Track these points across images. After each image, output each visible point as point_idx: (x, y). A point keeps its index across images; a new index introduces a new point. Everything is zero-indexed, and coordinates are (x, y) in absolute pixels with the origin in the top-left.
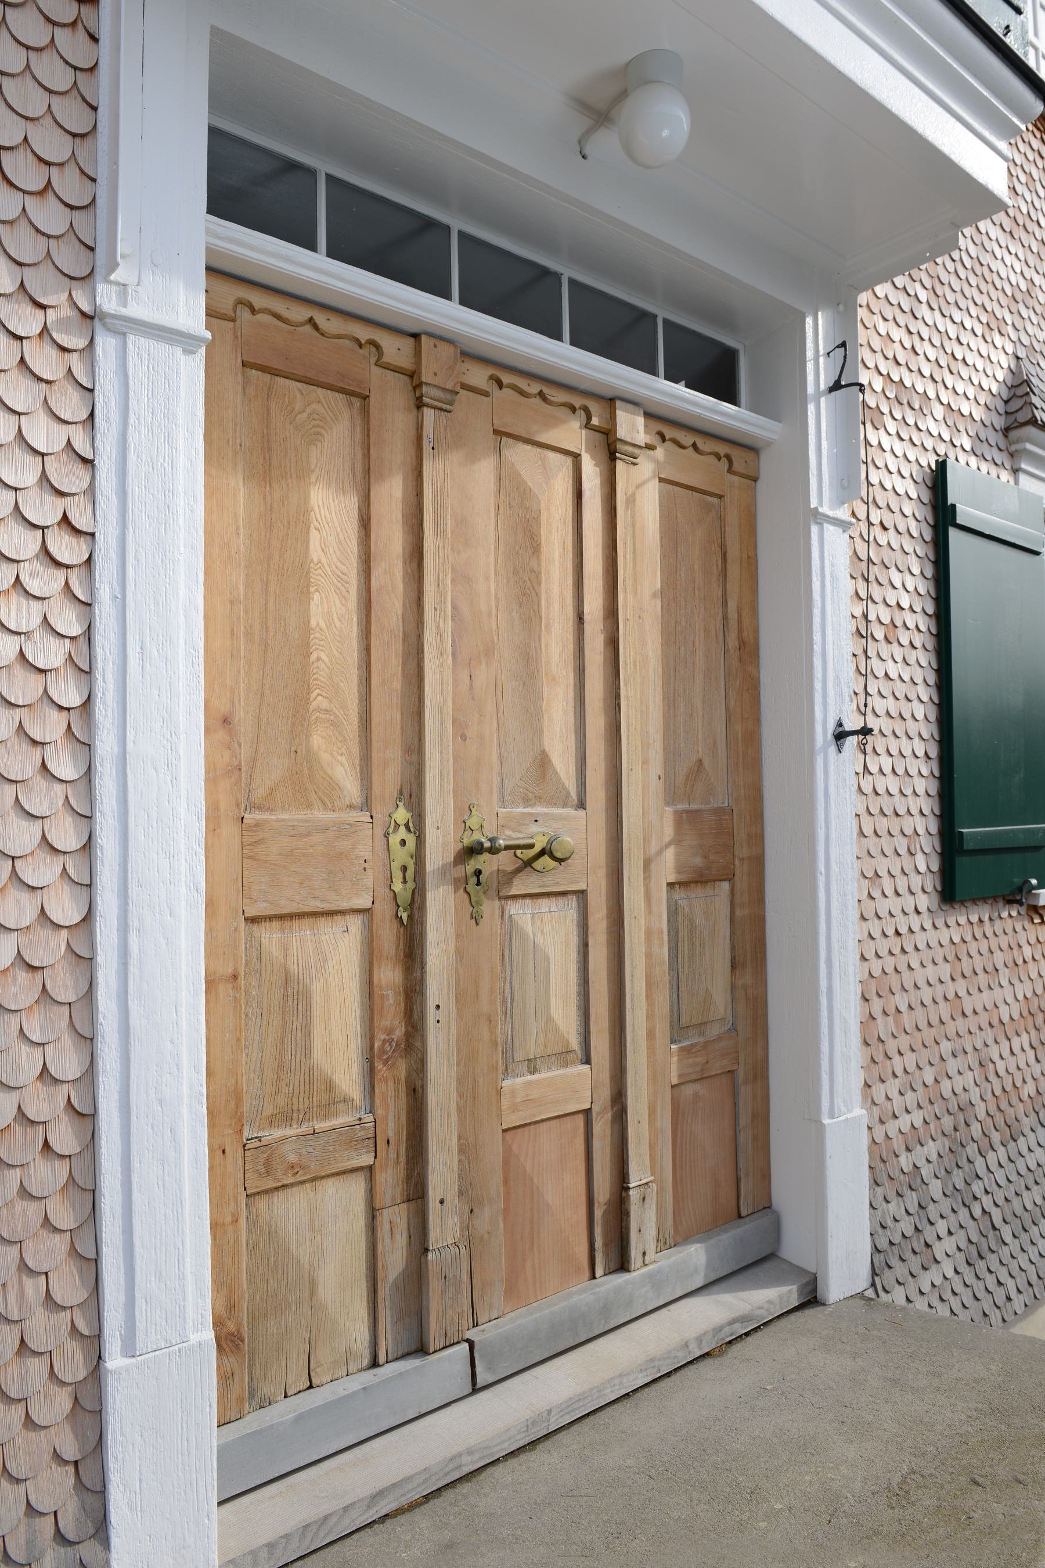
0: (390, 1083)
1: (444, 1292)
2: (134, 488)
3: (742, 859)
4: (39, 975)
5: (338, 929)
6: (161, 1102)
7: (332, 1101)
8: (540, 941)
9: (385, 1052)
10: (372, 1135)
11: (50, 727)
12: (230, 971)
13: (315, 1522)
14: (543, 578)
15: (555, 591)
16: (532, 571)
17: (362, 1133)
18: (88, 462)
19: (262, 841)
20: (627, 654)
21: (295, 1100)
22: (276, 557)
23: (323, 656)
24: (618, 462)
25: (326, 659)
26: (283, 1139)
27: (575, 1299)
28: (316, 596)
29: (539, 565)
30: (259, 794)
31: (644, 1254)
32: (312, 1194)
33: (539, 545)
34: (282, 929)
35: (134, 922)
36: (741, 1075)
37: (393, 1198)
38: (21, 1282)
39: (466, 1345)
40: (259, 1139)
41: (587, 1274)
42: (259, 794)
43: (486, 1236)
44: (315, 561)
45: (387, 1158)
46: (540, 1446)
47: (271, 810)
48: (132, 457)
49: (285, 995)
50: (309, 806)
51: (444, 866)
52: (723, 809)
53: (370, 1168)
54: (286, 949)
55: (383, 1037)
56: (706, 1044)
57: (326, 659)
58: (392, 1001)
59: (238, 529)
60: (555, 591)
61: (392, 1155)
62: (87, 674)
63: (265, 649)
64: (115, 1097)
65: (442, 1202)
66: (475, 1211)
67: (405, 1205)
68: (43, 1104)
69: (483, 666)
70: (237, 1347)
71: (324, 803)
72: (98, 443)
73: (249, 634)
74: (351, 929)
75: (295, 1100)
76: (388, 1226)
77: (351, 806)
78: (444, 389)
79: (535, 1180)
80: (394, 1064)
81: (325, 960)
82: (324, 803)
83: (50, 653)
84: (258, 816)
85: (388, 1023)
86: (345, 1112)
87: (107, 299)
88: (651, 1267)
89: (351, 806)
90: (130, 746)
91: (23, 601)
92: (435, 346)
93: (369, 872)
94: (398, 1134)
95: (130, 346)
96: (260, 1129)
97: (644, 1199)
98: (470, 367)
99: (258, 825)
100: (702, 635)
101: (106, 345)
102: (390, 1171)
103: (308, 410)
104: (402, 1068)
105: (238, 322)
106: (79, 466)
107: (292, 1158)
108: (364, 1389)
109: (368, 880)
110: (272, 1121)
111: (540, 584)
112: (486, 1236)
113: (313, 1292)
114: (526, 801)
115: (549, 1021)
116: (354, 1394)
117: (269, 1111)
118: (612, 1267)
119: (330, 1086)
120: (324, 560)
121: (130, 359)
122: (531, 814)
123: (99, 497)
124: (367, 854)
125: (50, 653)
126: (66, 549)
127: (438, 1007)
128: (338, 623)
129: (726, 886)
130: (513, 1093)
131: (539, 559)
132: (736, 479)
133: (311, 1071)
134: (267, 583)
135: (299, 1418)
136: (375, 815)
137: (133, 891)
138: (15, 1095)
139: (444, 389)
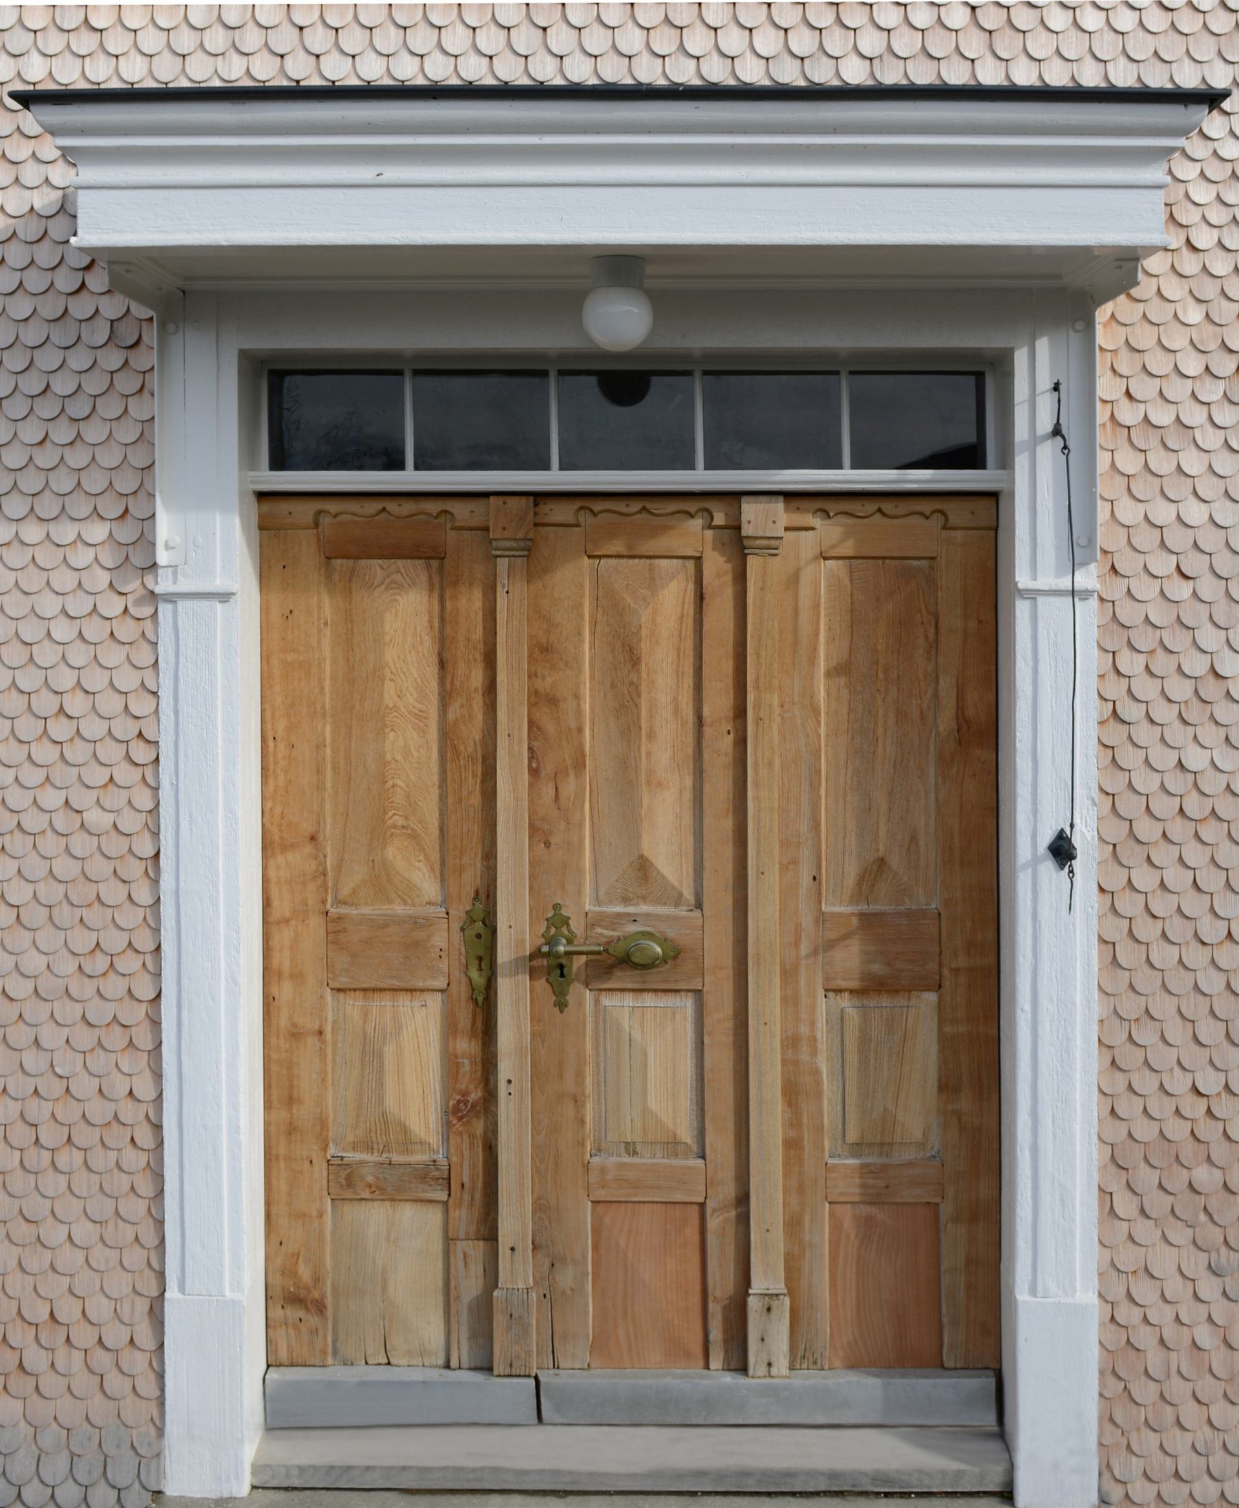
0: (465, 1137)
1: (509, 1328)
2: (183, 708)
3: (956, 971)
4: (127, 1031)
5: (416, 1003)
6: (205, 1127)
7: (408, 1141)
8: (637, 1035)
9: (460, 1111)
10: (445, 1175)
11: (135, 869)
12: (316, 1027)
13: (341, 1467)
14: (643, 688)
15: (664, 698)
16: (631, 683)
17: (437, 1173)
18: (155, 693)
19: (344, 931)
20: (759, 755)
21: (373, 1135)
22: (357, 707)
23: (399, 782)
24: (749, 558)
25: (403, 785)
26: (362, 1163)
27: (669, 1380)
28: (392, 735)
29: (639, 678)
30: (345, 892)
31: (770, 1364)
32: (391, 1212)
33: (639, 659)
34: (365, 998)
35: (185, 1003)
36: (946, 1210)
37: (467, 1233)
38: (116, 1223)
39: (533, 1381)
40: (342, 1158)
41: (701, 1363)
42: (345, 892)
43: (569, 1292)
44: (391, 705)
45: (461, 1198)
46: (570, 1498)
47: (356, 905)
48: (182, 685)
49: (364, 1051)
50: (390, 901)
51: (516, 960)
52: (923, 913)
53: (446, 1204)
54: (366, 1015)
55: (458, 1097)
56: (885, 1167)
57: (403, 785)
58: (467, 1068)
59: (322, 689)
60: (664, 698)
61: (466, 1197)
62: (156, 834)
63: (350, 780)
64: (174, 1118)
65: (513, 1249)
66: (556, 1266)
67: (481, 1243)
68: (129, 1112)
69: (572, 778)
70: (321, 1312)
71: (404, 901)
72: (161, 680)
73: (335, 769)
74: (429, 1003)
75: (373, 1135)
76: (462, 1256)
77: (430, 903)
78: (515, 540)
79: (630, 1255)
80: (468, 1122)
81: (400, 1028)
82: (404, 901)
83: (131, 822)
84: (343, 910)
85: (463, 1087)
86: (423, 1152)
87: (163, 586)
88: (774, 1381)
89: (430, 903)
90: (182, 884)
91: (116, 789)
92: (504, 503)
93: (445, 959)
94: (473, 1181)
95: (180, 609)
96: (344, 1150)
97: (769, 1309)
98: (552, 507)
99: (340, 918)
100: (891, 720)
101: (165, 610)
102: (464, 1211)
103: (387, 582)
104: (479, 1127)
105: (321, 528)
106: (151, 696)
107: (370, 1179)
108: (424, 1382)
109: (444, 966)
110: (354, 1147)
111: (639, 696)
112: (569, 1292)
113: (384, 1289)
114: (626, 900)
115: (646, 1111)
116: (413, 1383)
117: (350, 1138)
118: (733, 1365)
119: (405, 1130)
120: (399, 703)
121: (179, 618)
122: (629, 914)
123: (161, 715)
124: (444, 945)
125: (131, 822)
126: (141, 753)
127: (509, 1082)
128: (415, 754)
129: (932, 997)
130: (603, 1170)
131: (638, 671)
132: (959, 535)
133: (384, 1114)
134: (351, 727)
135: (362, 1384)
136: (451, 912)
137: (185, 982)
138: (113, 1104)
139: (515, 540)
